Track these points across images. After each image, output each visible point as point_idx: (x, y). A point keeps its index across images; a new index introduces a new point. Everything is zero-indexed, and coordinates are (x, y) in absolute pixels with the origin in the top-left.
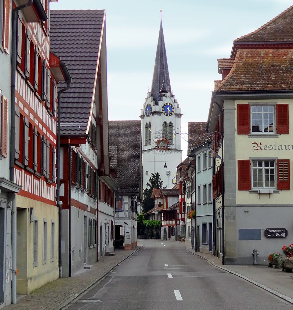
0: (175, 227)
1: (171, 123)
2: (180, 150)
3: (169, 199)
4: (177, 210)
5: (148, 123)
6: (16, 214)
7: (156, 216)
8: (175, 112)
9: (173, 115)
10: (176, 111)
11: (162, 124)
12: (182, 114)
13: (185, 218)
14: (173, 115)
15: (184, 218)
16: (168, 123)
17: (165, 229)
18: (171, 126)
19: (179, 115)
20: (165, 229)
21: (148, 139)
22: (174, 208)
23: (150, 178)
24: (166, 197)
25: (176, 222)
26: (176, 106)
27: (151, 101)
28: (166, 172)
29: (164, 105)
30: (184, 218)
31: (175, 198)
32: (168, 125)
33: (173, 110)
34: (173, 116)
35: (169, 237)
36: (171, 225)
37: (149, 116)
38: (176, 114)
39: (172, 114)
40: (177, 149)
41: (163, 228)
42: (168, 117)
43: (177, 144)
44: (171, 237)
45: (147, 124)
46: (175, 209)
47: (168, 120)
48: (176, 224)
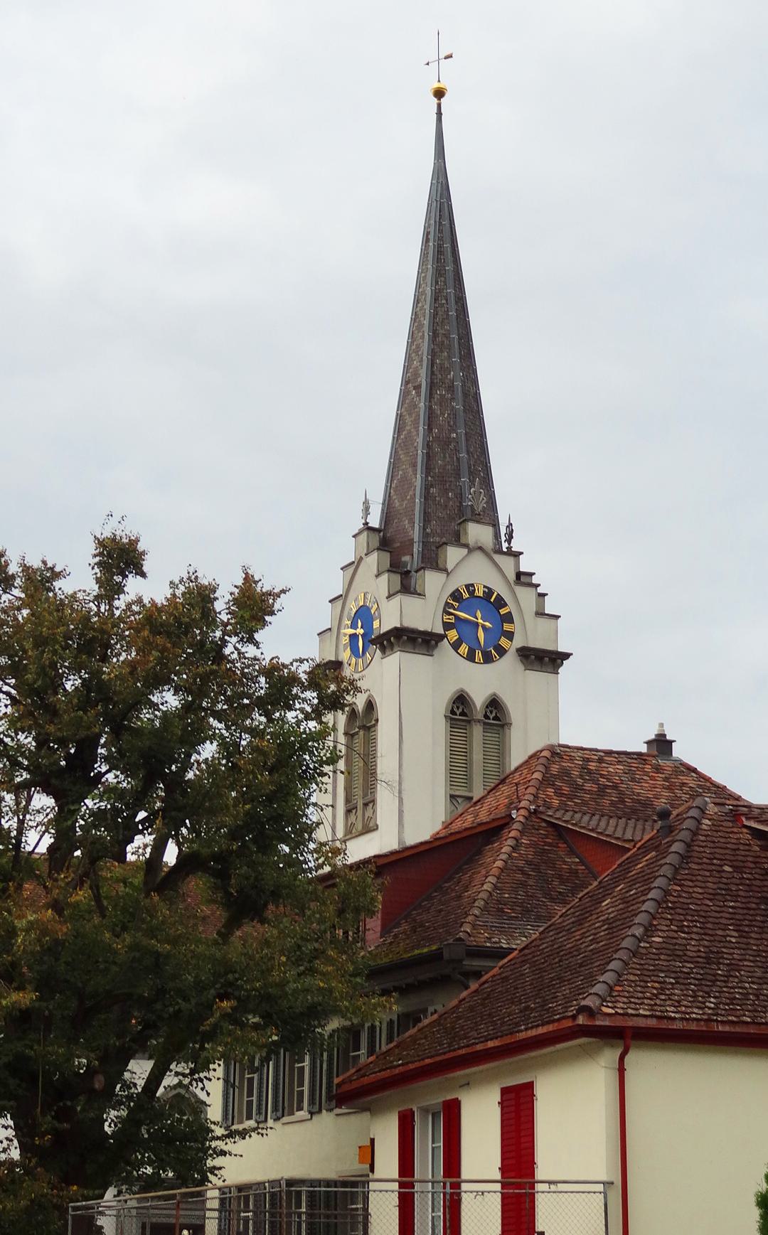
1: (494, 704)
8: (518, 642)
16: (479, 700)
19: (547, 660)
39: (502, 652)
47: (481, 682)
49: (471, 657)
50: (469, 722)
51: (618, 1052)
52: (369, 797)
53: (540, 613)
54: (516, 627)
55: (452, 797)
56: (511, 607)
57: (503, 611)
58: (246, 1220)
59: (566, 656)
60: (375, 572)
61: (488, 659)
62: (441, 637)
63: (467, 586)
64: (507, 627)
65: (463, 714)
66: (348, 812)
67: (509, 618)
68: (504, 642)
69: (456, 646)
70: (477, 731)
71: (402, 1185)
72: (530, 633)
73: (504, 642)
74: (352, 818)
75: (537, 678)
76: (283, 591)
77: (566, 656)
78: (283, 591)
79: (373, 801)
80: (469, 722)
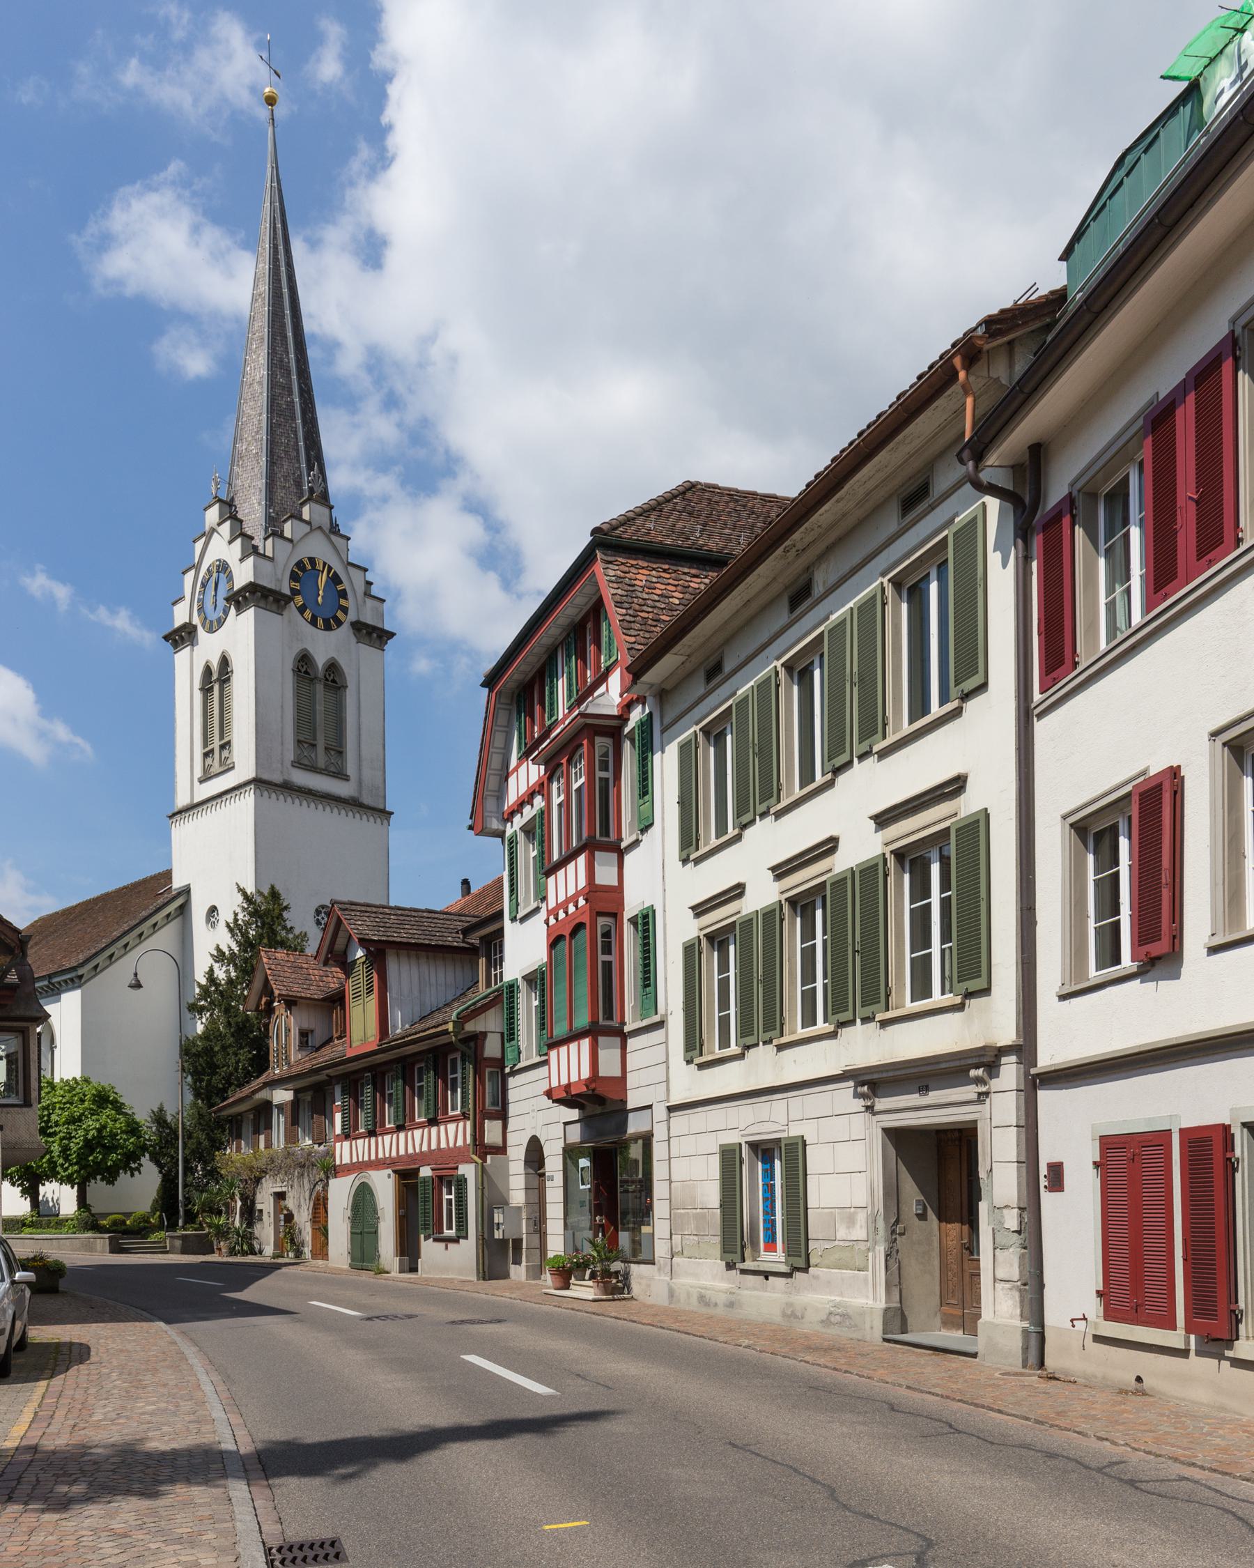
0: (468, 1171)
1: (333, 667)
2: (381, 807)
3: (401, 972)
4: (484, 1035)
5: (215, 665)
6: (1164, 881)
7: (280, 1123)
8: (352, 616)
9: (345, 629)
10: (359, 609)
11: (289, 664)
12: (387, 627)
13: (623, 1078)
14: (345, 629)
15: (618, 1073)
16: (320, 661)
17: (363, 1201)
18: (334, 681)
19: (376, 635)
20: (363, 1201)
21: (216, 744)
22: (463, 1019)
23: (236, 920)
24: (378, 953)
25: (478, 1133)
26: (360, 587)
27: (230, 542)
28: (313, 912)
29: (300, 564)
30: (618, 1073)
31: (424, 968)
32: (321, 675)
33: (342, 602)
34: (344, 633)
35: (408, 1251)
36: (422, 1158)
37: (221, 622)
38: (358, 627)
39: (339, 623)
40: (367, 800)
41: (340, 1192)
42: (321, 635)
43: (367, 774)
44: (429, 1249)
45: (208, 670)
46: (470, 1027)
47: (325, 647)
48: (481, 1148)
49: (313, 622)
50: (312, 680)
51: (575, 1025)
52: (226, 740)
53: (367, 594)
54: (350, 603)
55: (299, 741)
56: (345, 585)
57: (340, 588)
58: (450, 1201)
59: (391, 635)
60: (239, 556)
61: (328, 627)
62: (289, 599)
63: (310, 559)
64: (342, 602)
65: (306, 672)
66: (206, 755)
67: (343, 594)
68: (340, 614)
69: (302, 610)
70: (320, 688)
71: (543, 1175)
72: (359, 609)
73: (340, 614)
74: (209, 761)
75: (366, 651)
76: (136, 975)
77: (391, 635)
78: (136, 975)
79: (229, 743)
80: (312, 680)
